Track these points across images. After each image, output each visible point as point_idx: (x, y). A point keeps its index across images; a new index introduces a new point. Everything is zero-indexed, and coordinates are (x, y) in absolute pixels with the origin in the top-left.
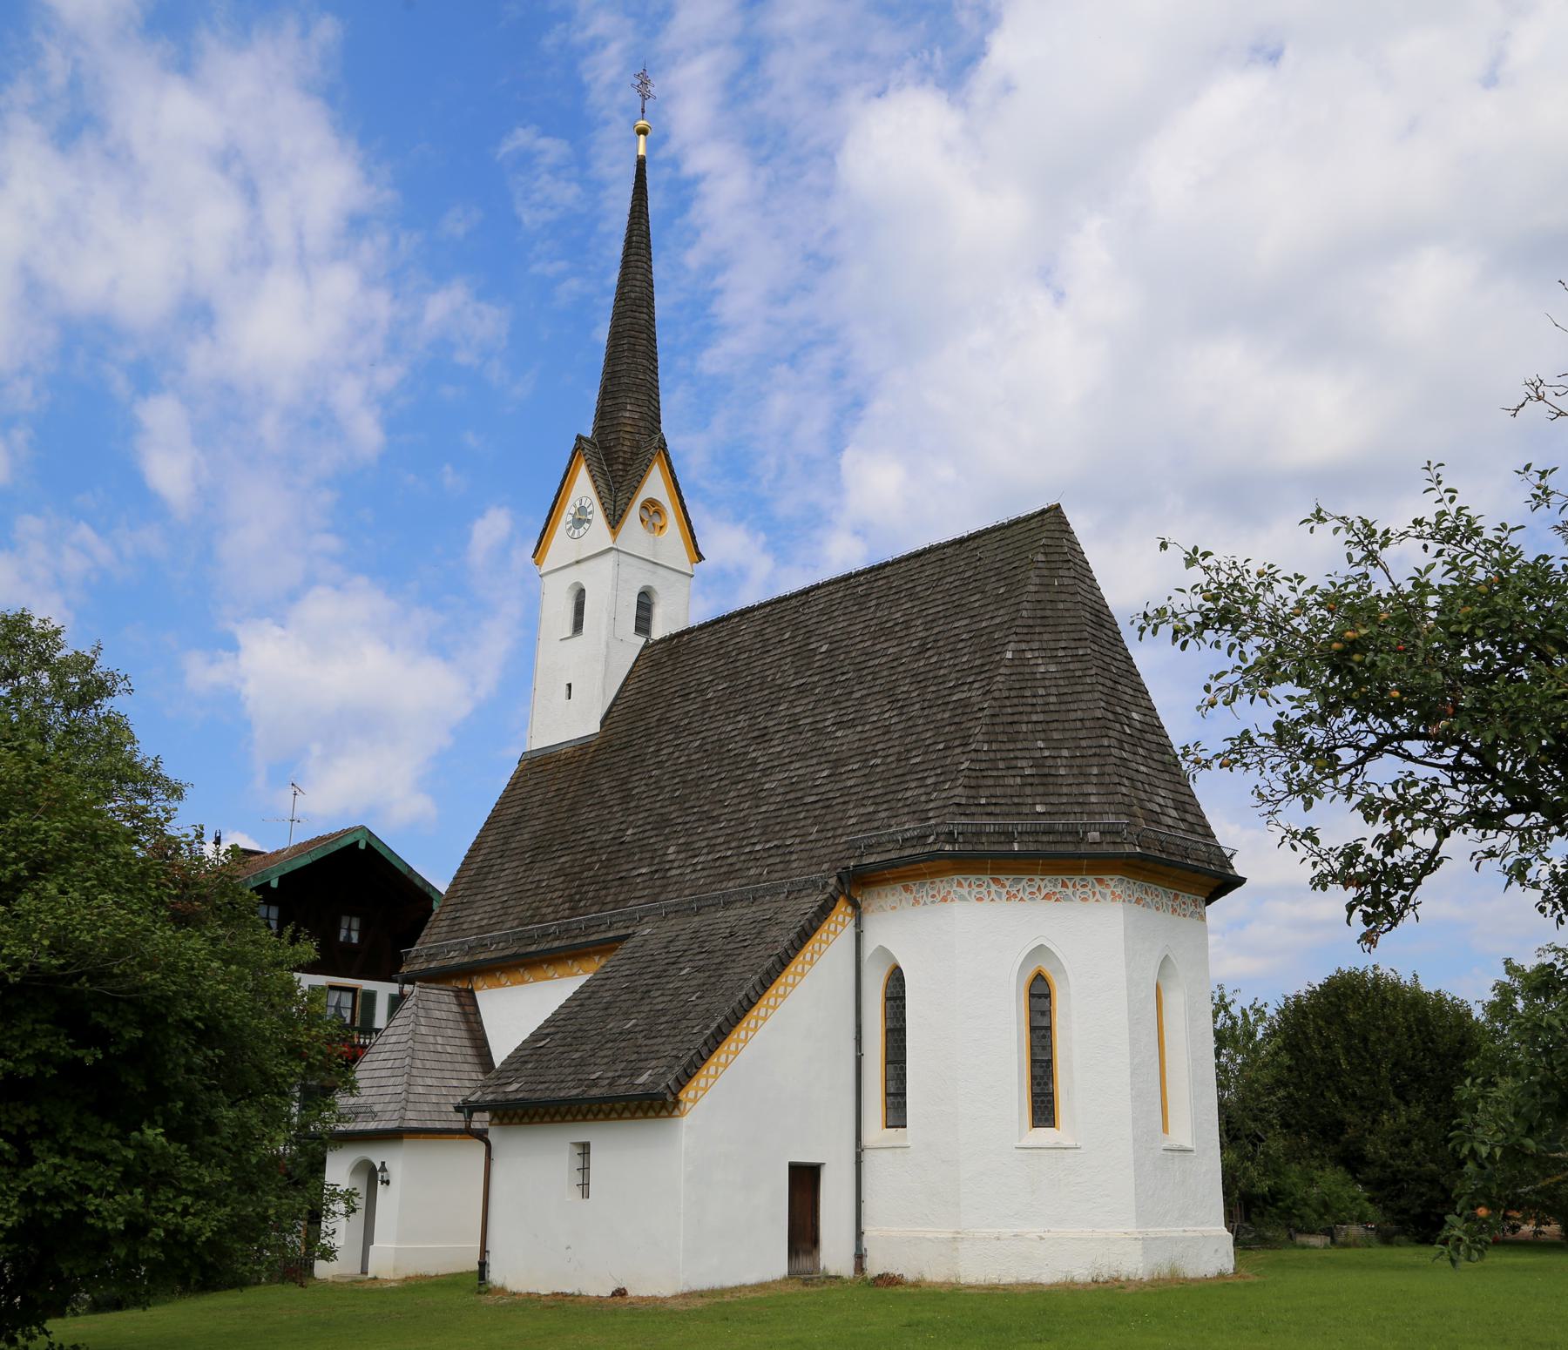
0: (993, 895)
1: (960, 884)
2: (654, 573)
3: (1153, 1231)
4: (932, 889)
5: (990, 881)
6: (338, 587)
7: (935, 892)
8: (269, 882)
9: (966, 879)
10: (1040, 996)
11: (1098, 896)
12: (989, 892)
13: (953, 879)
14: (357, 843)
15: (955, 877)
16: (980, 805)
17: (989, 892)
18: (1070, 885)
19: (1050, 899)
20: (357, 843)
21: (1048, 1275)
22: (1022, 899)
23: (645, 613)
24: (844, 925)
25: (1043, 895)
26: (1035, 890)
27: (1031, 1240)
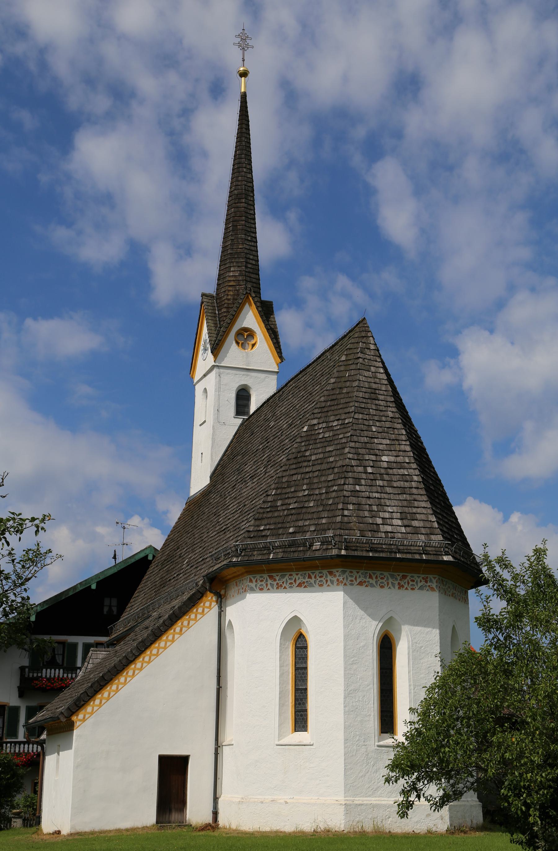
1: (251, 581)
2: (248, 375)
3: (359, 800)
4: (352, 576)
5: (328, 573)
6: (533, 290)
7: (293, 581)
8: (90, 586)
9: (313, 573)
10: (301, 648)
11: (329, 583)
12: (267, 585)
13: (305, 574)
14: (147, 556)
15: (249, 576)
16: (260, 530)
17: (267, 585)
19: (301, 586)
20: (147, 556)
21: (288, 827)
22: (285, 588)
23: (241, 402)
24: (210, 607)
25: (297, 584)
26: (293, 581)
27: (281, 804)
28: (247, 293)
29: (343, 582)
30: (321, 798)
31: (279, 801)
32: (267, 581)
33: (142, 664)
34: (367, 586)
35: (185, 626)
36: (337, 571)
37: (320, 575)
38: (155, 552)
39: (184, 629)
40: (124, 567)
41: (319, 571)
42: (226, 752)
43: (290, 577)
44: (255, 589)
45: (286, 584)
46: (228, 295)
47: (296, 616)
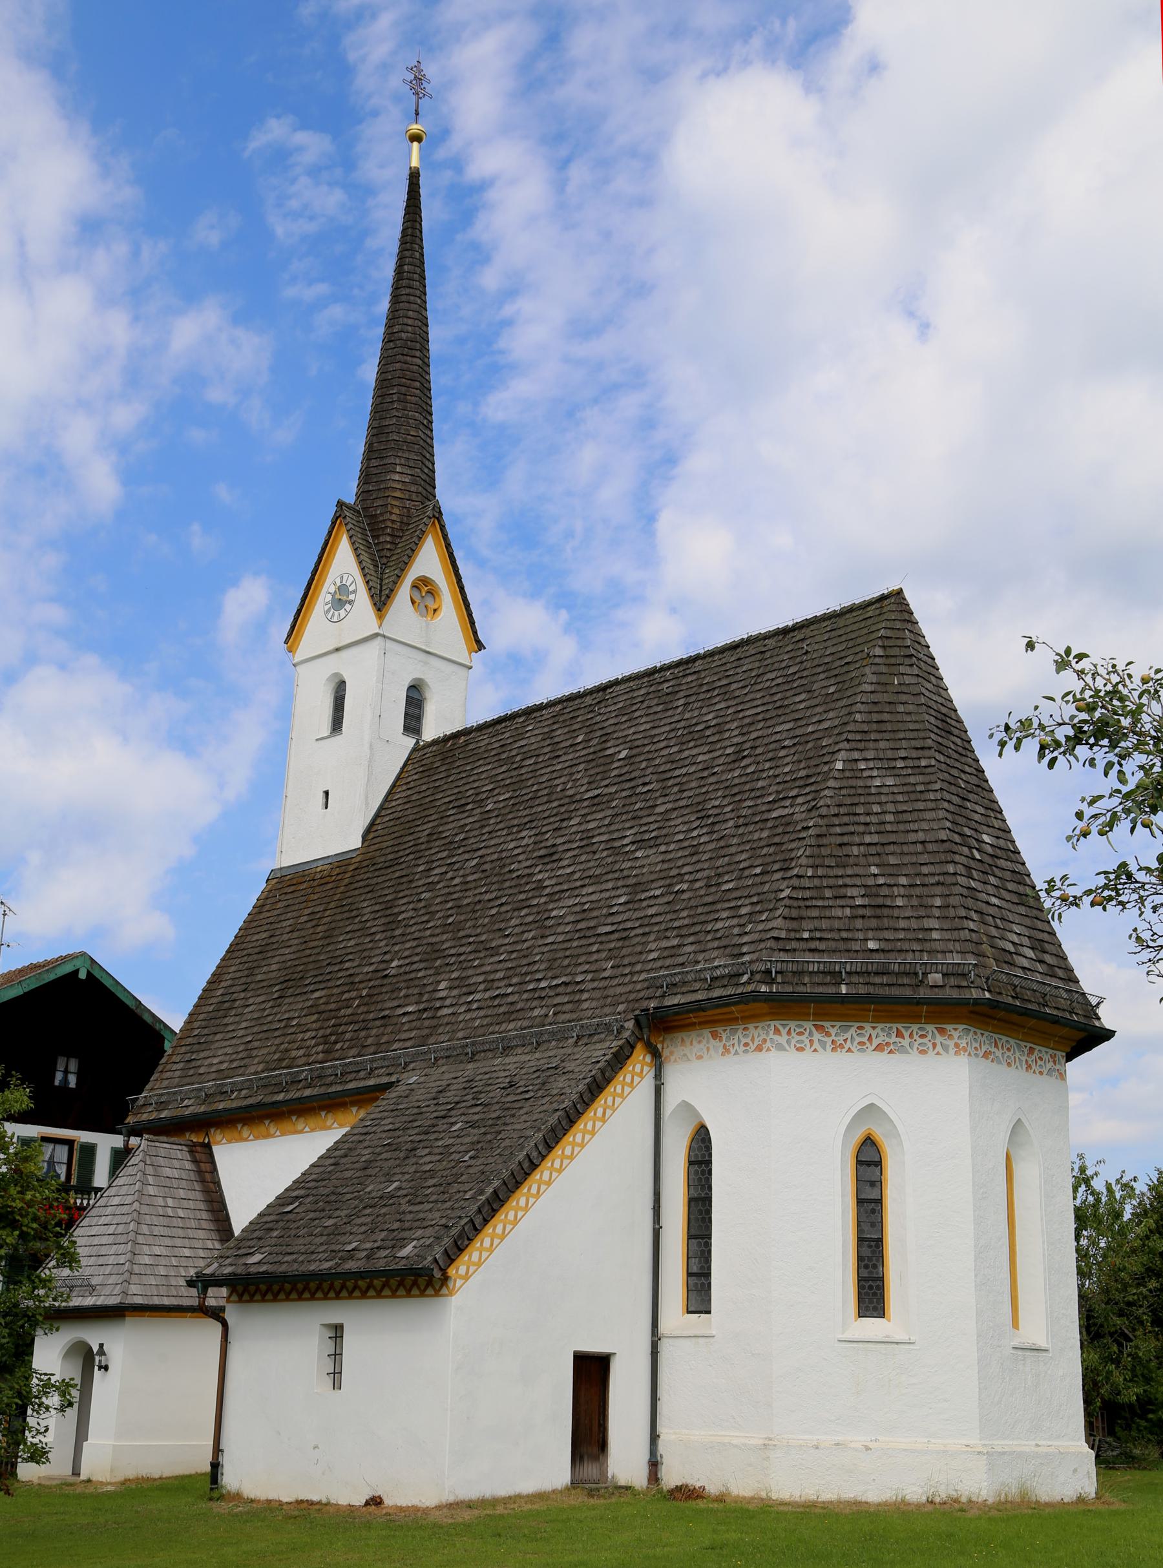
0: (816, 1045)
1: (777, 1031)
3: (1000, 1444)
5: (936, 1032)
6: (63, 667)
11: (939, 1048)
12: (811, 1041)
13: (769, 1026)
14: (76, 972)
15: (772, 1023)
17: (811, 1041)
18: (906, 1035)
19: (882, 1050)
20: (76, 972)
22: (849, 1050)
23: (415, 711)
24: (641, 1075)
25: (874, 1046)
26: (865, 1040)
27: (856, 1450)
28: (434, 516)
29: (966, 1051)
30: (933, 1441)
31: (853, 1445)
32: (811, 1034)
33: (551, 1173)
34: (992, 1061)
35: (608, 1107)
36: (955, 1029)
37: (921, 1033)
38: (91, 965)
39: (608, 1112)
40: (33, 986)
41: (919, 1025)
42: (665, 1347)
43: (859, 1032)
44: (787, 1047)
45: (852, 1043)
46: (391, 513)
47: (872, 1104)
